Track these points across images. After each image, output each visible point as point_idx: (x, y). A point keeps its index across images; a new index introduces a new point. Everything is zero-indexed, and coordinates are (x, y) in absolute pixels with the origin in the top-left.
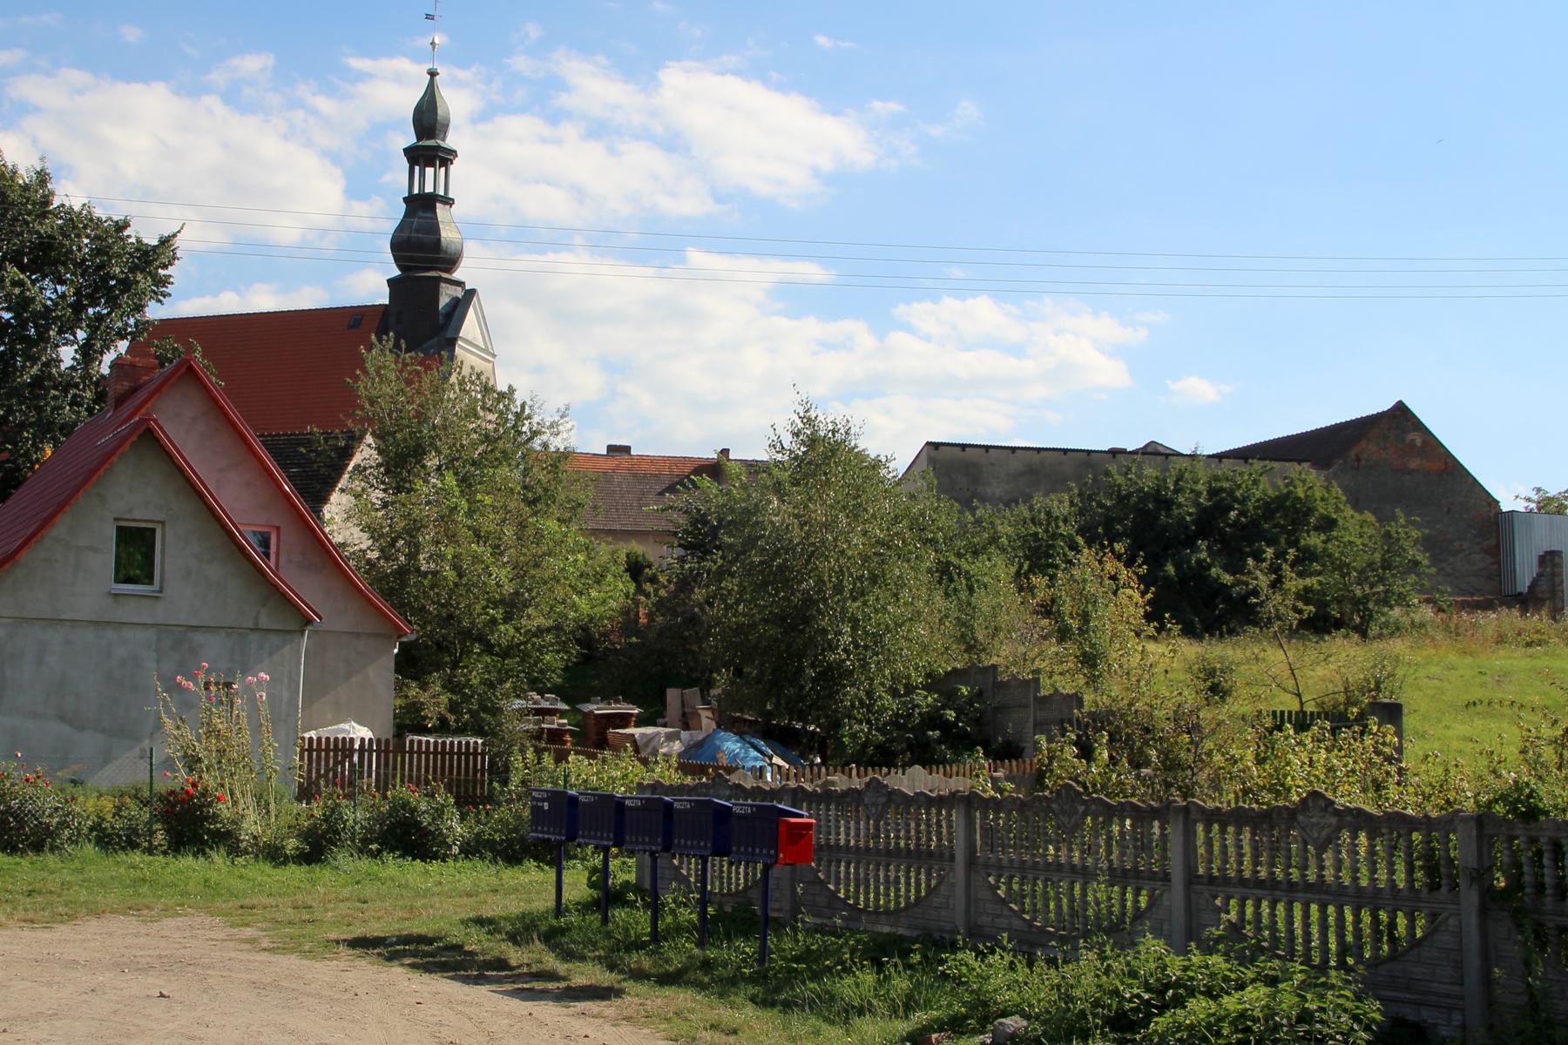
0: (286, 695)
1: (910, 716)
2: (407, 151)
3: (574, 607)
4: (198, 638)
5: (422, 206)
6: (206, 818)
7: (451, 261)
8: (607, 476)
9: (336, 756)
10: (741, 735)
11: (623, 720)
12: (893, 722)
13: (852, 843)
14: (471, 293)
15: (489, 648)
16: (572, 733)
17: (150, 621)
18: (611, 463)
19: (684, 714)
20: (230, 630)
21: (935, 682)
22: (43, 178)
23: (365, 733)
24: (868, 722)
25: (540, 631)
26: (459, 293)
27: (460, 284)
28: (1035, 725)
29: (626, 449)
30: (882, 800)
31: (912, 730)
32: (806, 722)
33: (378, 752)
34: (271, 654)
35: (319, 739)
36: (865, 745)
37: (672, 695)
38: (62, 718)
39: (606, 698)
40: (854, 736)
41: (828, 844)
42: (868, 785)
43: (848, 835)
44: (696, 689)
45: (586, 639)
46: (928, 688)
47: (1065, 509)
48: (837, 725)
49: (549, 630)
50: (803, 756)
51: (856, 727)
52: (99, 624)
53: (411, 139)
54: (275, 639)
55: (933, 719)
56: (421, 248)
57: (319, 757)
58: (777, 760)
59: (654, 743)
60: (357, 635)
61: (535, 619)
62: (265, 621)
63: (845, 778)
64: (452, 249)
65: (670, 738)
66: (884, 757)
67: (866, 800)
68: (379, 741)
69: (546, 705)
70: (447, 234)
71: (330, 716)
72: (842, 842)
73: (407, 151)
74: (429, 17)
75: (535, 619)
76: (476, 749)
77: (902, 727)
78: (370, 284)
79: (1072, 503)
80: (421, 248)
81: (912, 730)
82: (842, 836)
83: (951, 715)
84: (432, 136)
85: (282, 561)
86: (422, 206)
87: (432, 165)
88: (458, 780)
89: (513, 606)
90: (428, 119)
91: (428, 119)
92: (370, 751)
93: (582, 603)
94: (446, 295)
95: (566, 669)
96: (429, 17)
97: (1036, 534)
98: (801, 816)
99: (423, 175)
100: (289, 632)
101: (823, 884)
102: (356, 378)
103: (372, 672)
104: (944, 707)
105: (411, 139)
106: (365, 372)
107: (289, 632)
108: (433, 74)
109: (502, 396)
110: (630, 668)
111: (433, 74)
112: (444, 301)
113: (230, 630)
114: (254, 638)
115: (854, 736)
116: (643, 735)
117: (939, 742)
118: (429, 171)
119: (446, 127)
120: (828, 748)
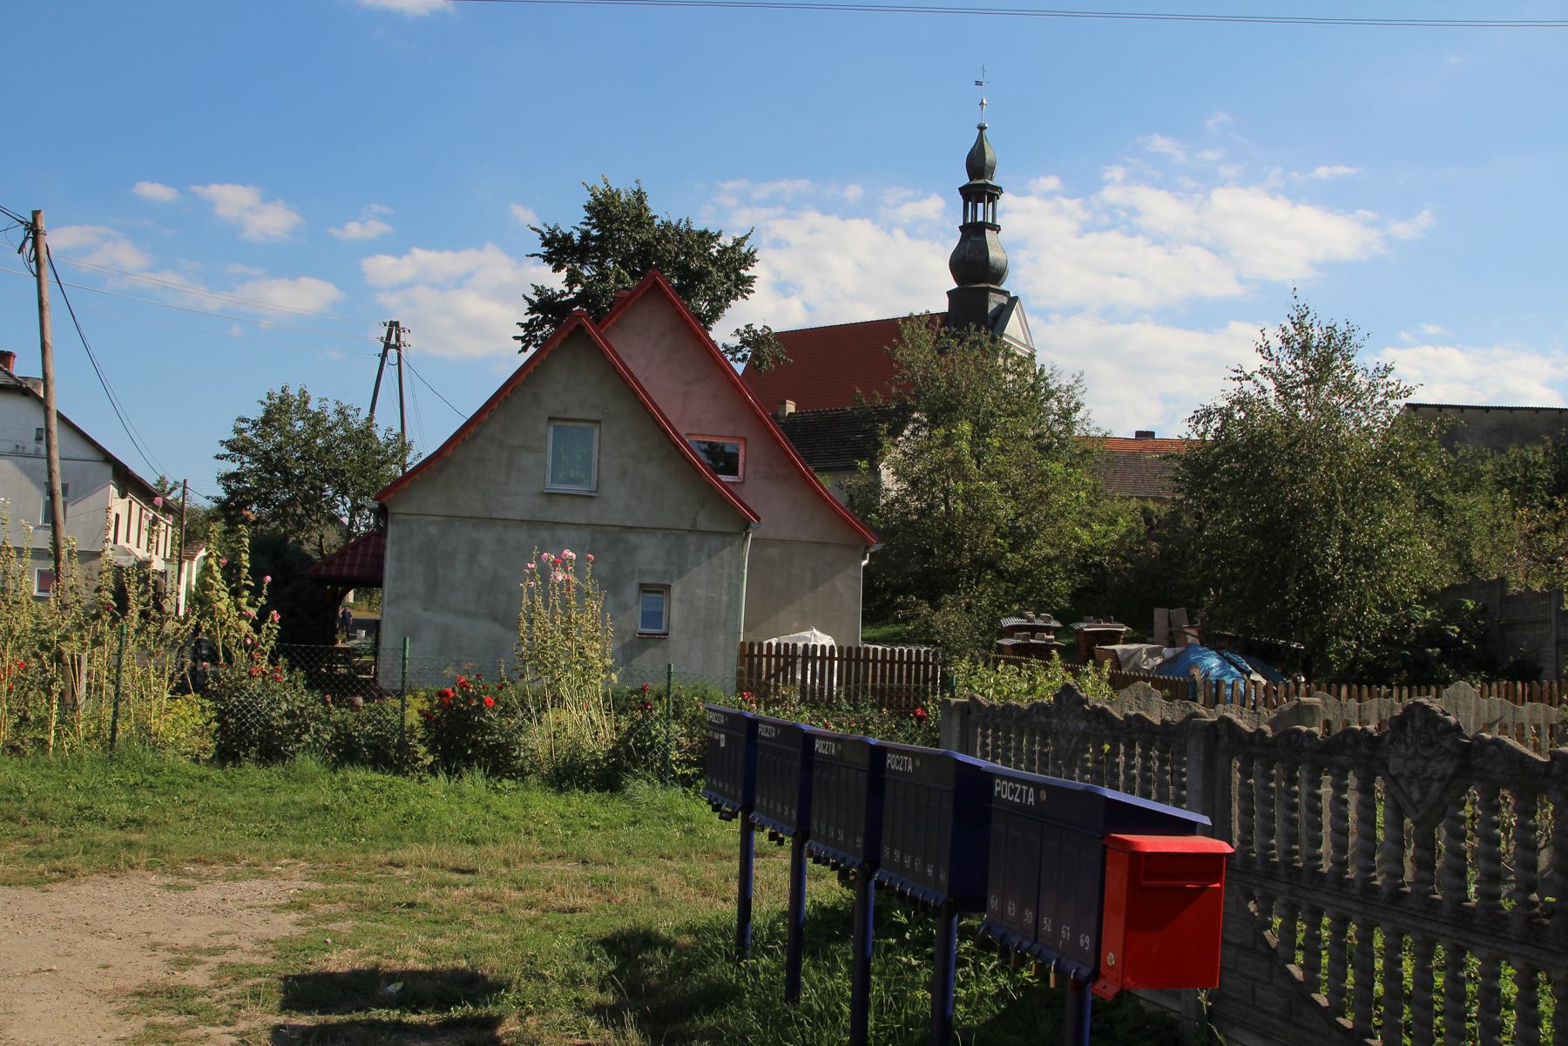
0: (725, 598)
1: (1405, 631)
2: (962, 190)
3: (1077, 539)
4: (633, 538)
5: (974, 232)
6: (472, 728)
7: (997, 275)
8: (1134, 456)
9: (777, 662)
10: (1219, 651)
11: (1113, 638)
12: (1385, 640)
13: (1351, 873)
14: (1015, 299)
15: (1000, 575)
16: (1059, 649)
17: (584, 521)
18: (1139, 445)
19: (1171, 634)
20: (666, 531)
21: (1429, 597)
22: (640, 196)
23: (826, 640)
24: (1358, 638)
25: (1049, 561)
26: (1005, 300)
27: (1005, 293)
28: (1558, 643)
29: (1151, 434)
30: (1446, 767)
31: (1409, 646)
32: (1289, 639)
33: (840, 659)
34: (709, 556)
35: (778, 645)
36: (1354, 663)
37: (1160, 615)
38: (494, 617)
39: (1099, 616)
40: (1341, 652)
41: (1288, 865)
42: (1399, 723)
43: (1340, 848)
44: (1183, 610)
45: (1084, 563)
46: (1427, 604)
47: (1540, 457)
48: (1322, 642)
49: (1056, 558)
50: (1285, 674)
51: (1344, 643)
52: (532, 524)
53: (965, 180)
54: (714, 542)
55: (1433, 635)
56: (975, 268)
57: (892, 669)
58: (1256, 677)
59: (1136, 658)
60: (824, 545)
61: (1041, 549)
62: (703, 523)
63: (1332, 700)
64: (999, 264)
65: (1151, 654)
66: (1415, 661)
67: (1394, 764)
68: (841, 649)
69: (1039, 622)
70: (994, 254)
71: (795, 625)
72: (1326, 866)
73: (962, 190)
74: (978, 83)
75: (1041, 549)
76: (926, 659)
77: (1398, 644)
78: (933, 291)
79: (1546, 454)
80: (975, 268)
81: (1409, 646)
82: (1326, 848)
83: (1454, 630)
84: (982, 176)
85: (749, 472)
86: (974, 232)
87: (982, 201)
88: (891, 689)
89: (1019, 539)
90: (977, 164)
91: (977, 164)
92: (832, 659)
93: (1085, 536)
94: (994, 302)
95: (1072, 595)
96: (978, 83)
97: (1514, 478)
98: (1187, 828)
99: (975, 209)
100: (728, 534)
101: (1276, 959)
102: (894, 347)
103: (839, 582)
104: (1444, 622)
105: (965, 180)
106: (901, 340)
107: (728, 534)
108: (982, 128)
109: (1021, 361)
110: (1121, 594)
111: (982, 128)
112: (992, 306)
113: (666, 531)
114: (692, 540)
115: (1341, 652)
116: (1126, 651)
117: (1440, 660)
118: (980, 206)
119: (992, 169)
120: (1314, 666)
